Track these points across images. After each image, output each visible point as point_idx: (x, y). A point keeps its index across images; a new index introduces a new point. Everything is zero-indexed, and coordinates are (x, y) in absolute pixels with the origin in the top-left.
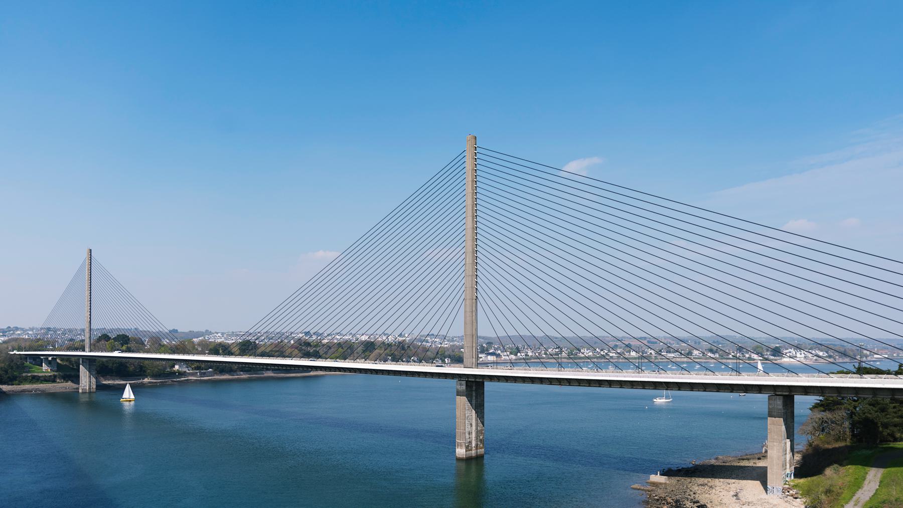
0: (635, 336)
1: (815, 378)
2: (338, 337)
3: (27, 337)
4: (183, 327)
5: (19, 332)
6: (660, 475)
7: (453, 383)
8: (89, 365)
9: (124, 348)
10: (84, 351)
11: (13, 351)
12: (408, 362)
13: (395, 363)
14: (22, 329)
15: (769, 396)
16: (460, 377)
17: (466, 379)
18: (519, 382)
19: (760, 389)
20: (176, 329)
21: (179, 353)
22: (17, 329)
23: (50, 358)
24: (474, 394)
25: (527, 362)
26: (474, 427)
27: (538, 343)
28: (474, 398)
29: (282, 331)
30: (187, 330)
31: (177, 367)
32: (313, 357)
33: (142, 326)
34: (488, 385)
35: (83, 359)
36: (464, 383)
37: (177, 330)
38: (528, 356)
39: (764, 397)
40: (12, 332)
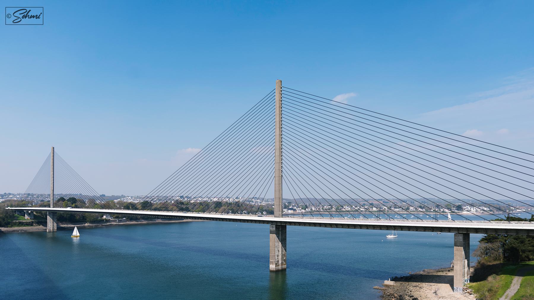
0: (376, 199)
1: (482, 223)
2: (200, 199)
3: (16, 199)
4: (108, 193)
5: (11, 196)
6: (390, 280)
7: (268, 226)
8: (53, 216)
9: (73, 205)
10: (50, 207)
11: (8, 207)
12: (241, 214)
13: (233, 214)
14: (13, 194)
15: (455, 234)
16: (272, 223)
17: (276, 224)
18: (307, 226)
19: (449, 229)
20: (104, 194)
21: (106, 209)
22: (10, 194)
23: (30, 212)
24: (280, 233)
25: (312, 214)
26: (280, 252)
27: (318, 203)
28: (280, 235)
29: (167, 196)
30: (110, 195)
31: (105, 217)
32: (185, 211)
33: (84, 192)
34: (289, 228)
35: (49, 212)
36: (274, 226)
37: (105, 195)
38: (313, 210)
39: (452, 234)
40: (7, 196)
